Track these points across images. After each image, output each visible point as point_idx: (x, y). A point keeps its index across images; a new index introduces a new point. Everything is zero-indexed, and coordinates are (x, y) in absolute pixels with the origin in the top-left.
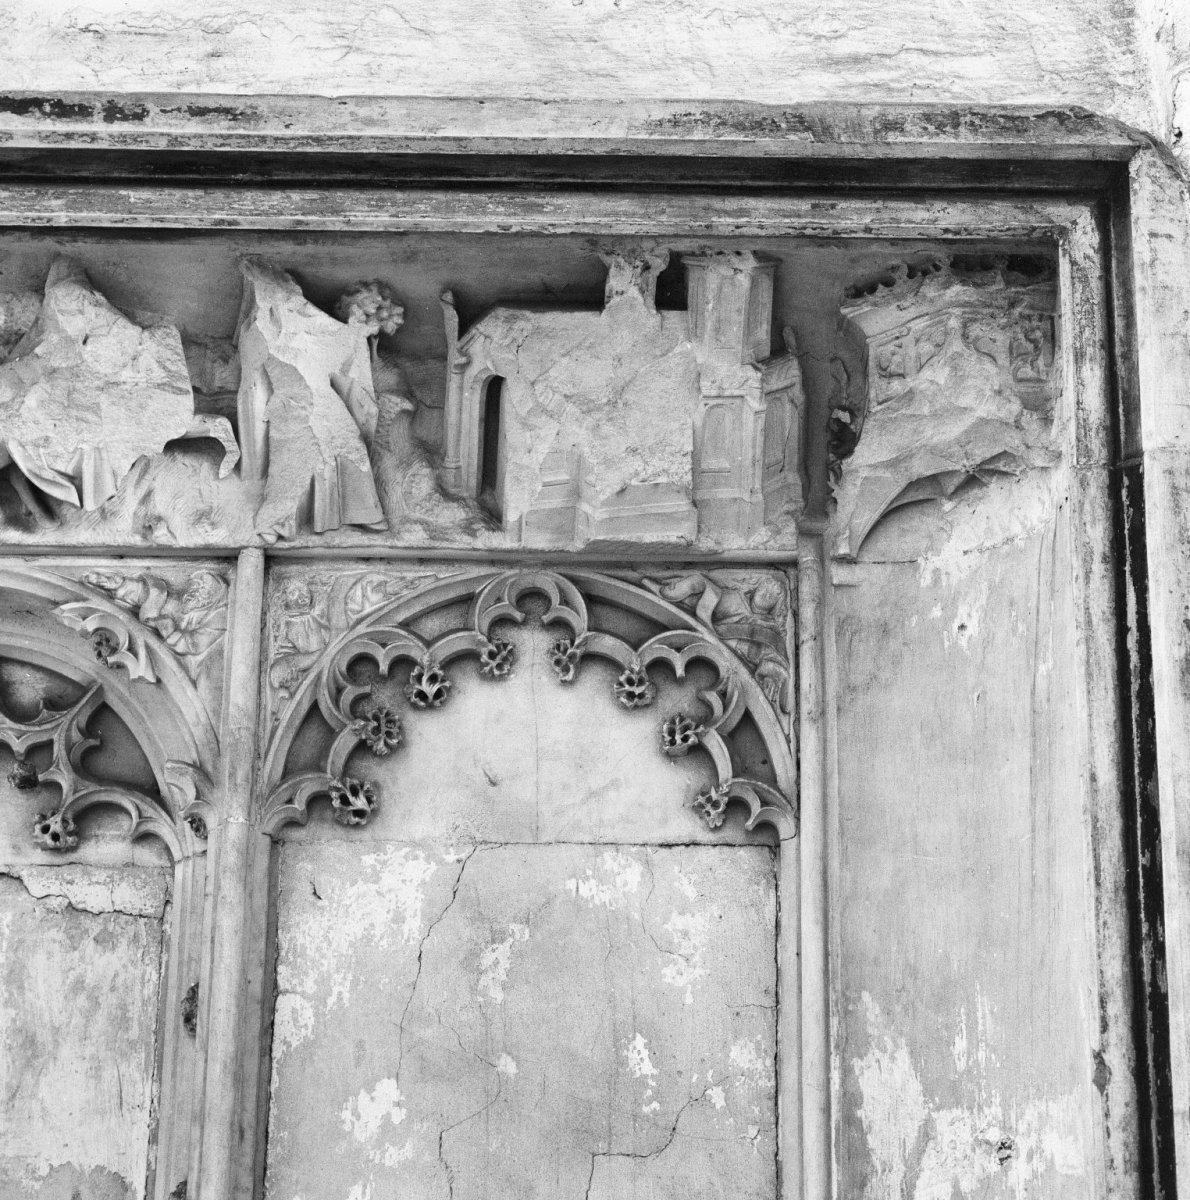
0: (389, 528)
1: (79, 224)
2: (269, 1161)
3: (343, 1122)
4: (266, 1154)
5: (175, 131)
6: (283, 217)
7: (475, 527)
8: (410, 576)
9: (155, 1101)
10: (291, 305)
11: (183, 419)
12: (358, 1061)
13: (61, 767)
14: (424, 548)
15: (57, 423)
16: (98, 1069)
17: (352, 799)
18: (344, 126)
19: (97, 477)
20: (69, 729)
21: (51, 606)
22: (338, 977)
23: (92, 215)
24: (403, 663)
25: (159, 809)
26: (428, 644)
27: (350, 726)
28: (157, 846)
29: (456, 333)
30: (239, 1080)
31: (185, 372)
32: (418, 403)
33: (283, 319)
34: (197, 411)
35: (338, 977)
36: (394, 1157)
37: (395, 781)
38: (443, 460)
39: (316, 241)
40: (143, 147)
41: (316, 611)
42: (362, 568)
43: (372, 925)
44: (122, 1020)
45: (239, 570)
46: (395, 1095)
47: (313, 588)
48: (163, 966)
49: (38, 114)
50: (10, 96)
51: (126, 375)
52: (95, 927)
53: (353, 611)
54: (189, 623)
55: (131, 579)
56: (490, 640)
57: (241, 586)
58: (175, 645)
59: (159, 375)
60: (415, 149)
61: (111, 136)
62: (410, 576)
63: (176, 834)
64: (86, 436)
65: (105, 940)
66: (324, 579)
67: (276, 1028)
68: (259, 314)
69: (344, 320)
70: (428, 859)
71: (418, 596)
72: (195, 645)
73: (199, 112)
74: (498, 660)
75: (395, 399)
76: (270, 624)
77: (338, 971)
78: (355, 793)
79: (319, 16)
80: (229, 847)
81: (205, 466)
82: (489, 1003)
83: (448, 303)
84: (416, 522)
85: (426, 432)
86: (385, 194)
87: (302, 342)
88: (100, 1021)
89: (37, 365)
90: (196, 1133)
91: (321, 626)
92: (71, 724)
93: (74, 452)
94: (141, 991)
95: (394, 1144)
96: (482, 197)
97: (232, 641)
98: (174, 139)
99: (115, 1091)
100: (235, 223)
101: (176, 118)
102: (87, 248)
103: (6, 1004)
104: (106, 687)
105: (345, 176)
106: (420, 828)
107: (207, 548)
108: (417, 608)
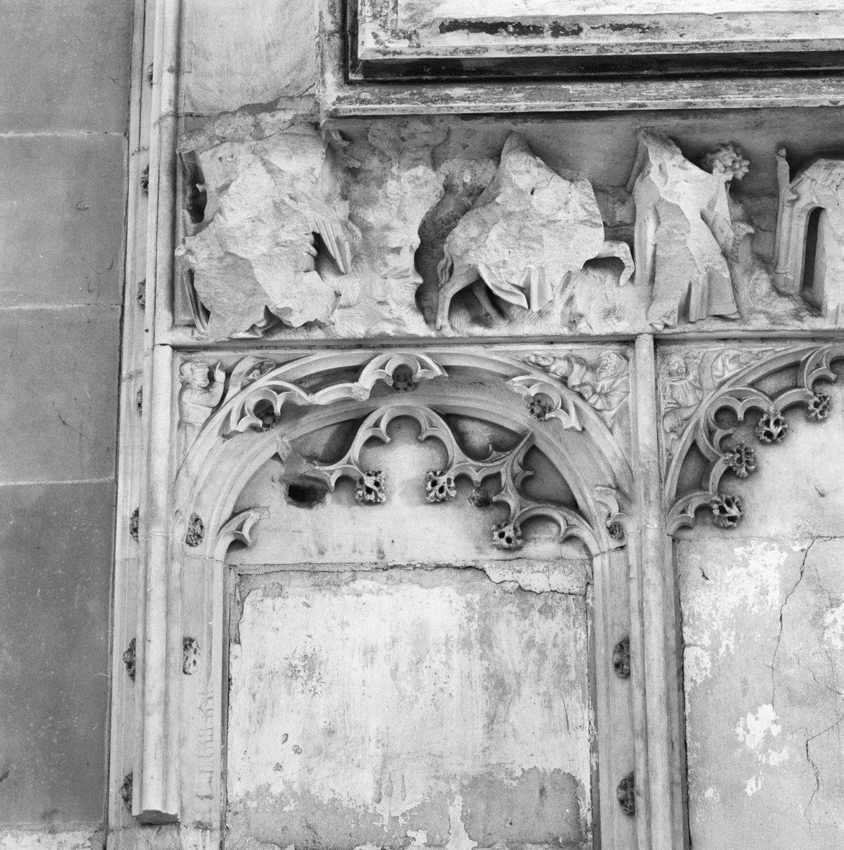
0: (741, 317)
1: (534, 110)
2: (689, 764)
3: (738, 735)
4: (686, 759)
5: (602, 42)
6: (677, 100)
7: (802, 314)
8: (755, 350)
9: (592, 722)
10: (674, 162)
11: (597, 244)
12: (744, 692)
13: (509, 491)
14: (767, 331)
15: (511, 250)
16: (550, 701)
17: (728, 509)
18: (721, 34)
19: (541, 288)
20: (512, 465)
21: (502, 379)
22: (725, 634)
23: (543, 103)
24: (754, 412)
25: (581, 519)
26: (773, 397)
27: (723, 458)
29: (788, 178)
30: (669, 709)
31: (598, 212)
32: (757, 227)
33: (669, 172)
34: (606, 239)
35: (725, 634)
36: (776, 759)
38: (775, 268)
39: (695, 116)
40: (580, 54)
41: (691, 378)
42: (722, 345)
43: (746, 597)
44: (563, 667)
45: (637, 350)
46: (773, 716)
47: (687, 360)
48: (589, 628)
49: (505, 33)
50: (484, 21)
51: (561, 215)
52: (539, 603)
53: (717, 377)
54: (603, 388)
55: (560, 359)
56: (815, 394)
57: (640, 361)
58: (595, 403)
59: (582, 215)
60: (772, 49)
61: (557, 47)
62: (755, 350)
63: (594, 536)
64: (533, 259)
65: (546, 611)
66: (695, 354)
67: (685, 670)
68: (652, 169)
69: (710, 171)
70: (781, 549)
71: (762, 365)
72: (609, 403)
73: (618, 28)
74: (821, 407)
75: (743, 226)
76: (660, 388)
77: (724, 630)
78: (729, 505)
80: (649, 545)
81: (609, 278)
82: (832, 650)
83: (782, 156)
84: (760, 312)
85: (765, 249)
86: (750, 82)
87: (683, 187)
88: (548, 669)
89: (497, 210)
90: (639, 745)
91: (696, 388)
92: (513, 461)
93: (524, 271)
94: (575, 647)
95: (775, 750)
96: (819, 81)
97: (636, 400)
98: (601, 48)
99: (563, 716)
100: (644, 105)
101: (602, 32)
102: (532, 127)
103: (481, 658)
104: (536, 434)
105: (720, 69)
106: (773, 528)
107: (614, 335)
108: (761, 373)
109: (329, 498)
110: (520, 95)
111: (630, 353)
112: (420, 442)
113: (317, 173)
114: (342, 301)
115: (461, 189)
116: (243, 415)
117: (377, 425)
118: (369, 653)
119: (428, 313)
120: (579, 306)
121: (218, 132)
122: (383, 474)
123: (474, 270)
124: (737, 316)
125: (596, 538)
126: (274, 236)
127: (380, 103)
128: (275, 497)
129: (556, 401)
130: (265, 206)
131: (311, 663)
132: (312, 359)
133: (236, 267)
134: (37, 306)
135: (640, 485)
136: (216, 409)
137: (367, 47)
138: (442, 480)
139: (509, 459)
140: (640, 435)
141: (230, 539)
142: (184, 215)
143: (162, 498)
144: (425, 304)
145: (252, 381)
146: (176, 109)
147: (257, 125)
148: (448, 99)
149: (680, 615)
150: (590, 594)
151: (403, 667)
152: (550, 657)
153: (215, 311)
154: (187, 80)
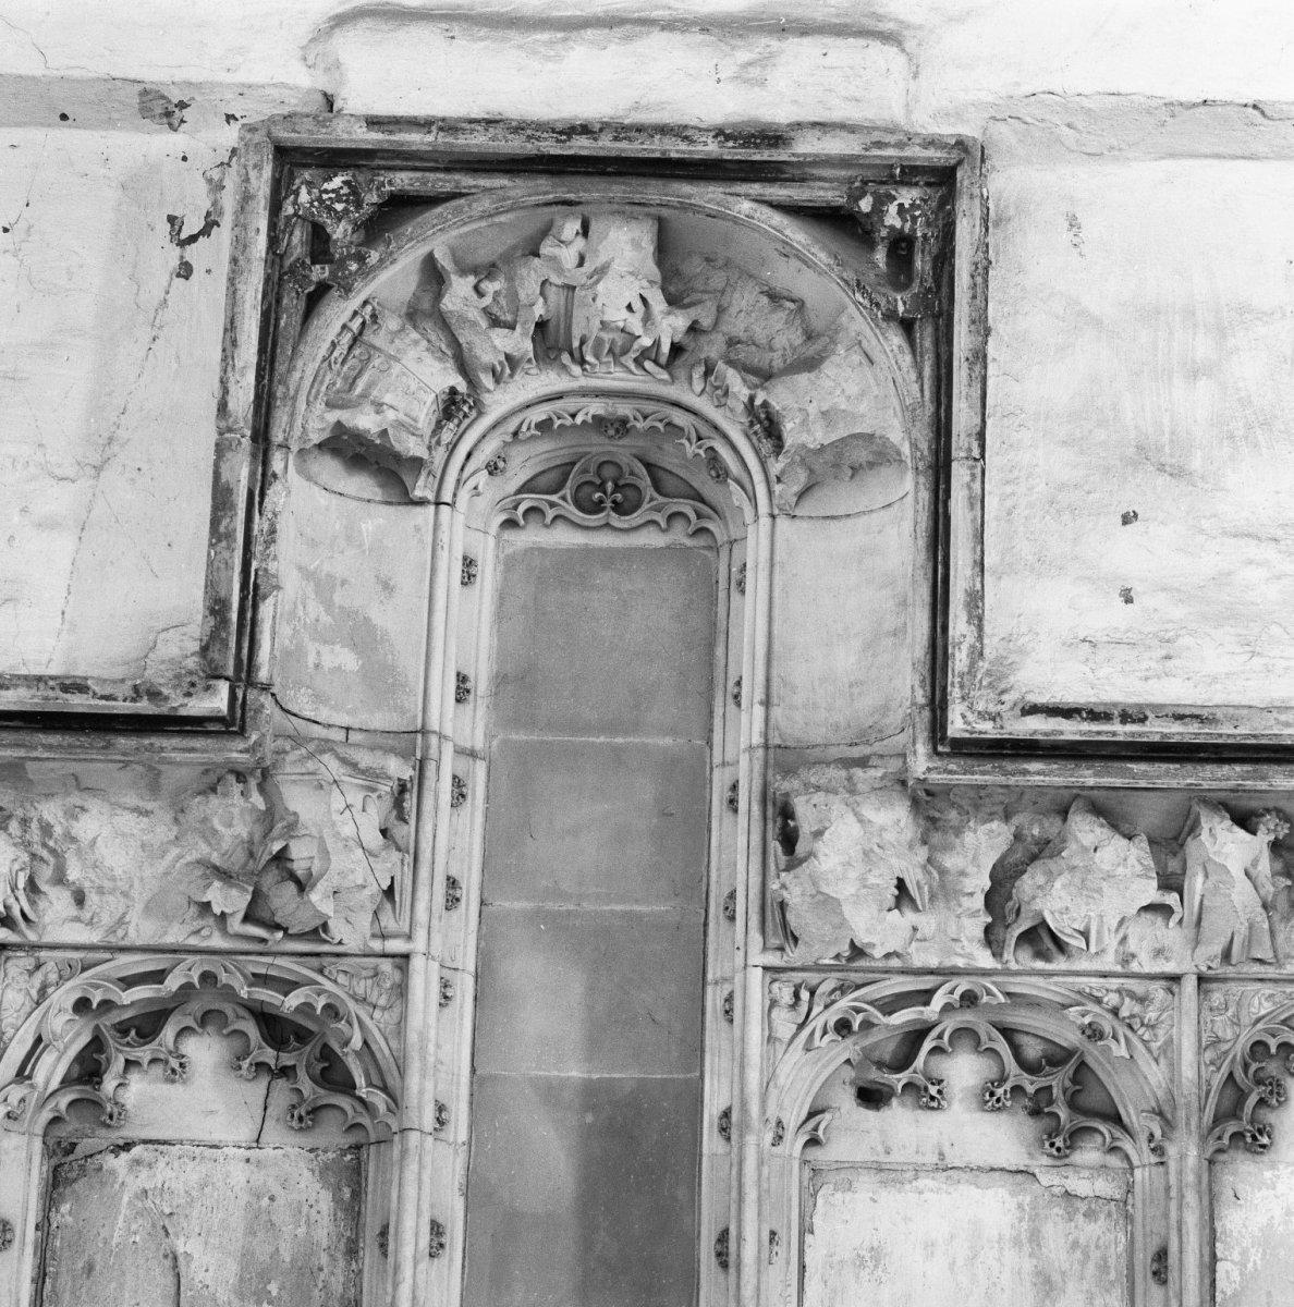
5: (1166, 730)
8: (1288, 990)
10: (1222, 825)
11: (1150, 892)
17: (1259, 1137)
27: (1256, 1091)
28: (1120, 1155)
31: (1153, 866)
35: (1253, 1251)
37: (1282, 1122)
40: (1145, 739)
41: (1229, 1013)
42: (1259, 985)
44: (1104, 1267)
52: (1083, 1207)
57: (1185, 1000)
59: (1139, 868)
65: (1090, 1215)
69: (1254, 833)
73: (1180, 717)
78: (1261, 1134)
79: (1232, 630)
81: (1159, 920)
87: (1230, 848)
88: (1091, 1268)
89: (1063, 863)
97: (1180, 1034)
98: (1164, 735)
109: (894, 1102)
110: (1090, 772)
111: (1175, 988)
112: (979, 1052)
113: (902, 824)
114: (919, 935)
115: (1029, 839)
116: (825, 1033)
117: (940, 1037)
118: (930, 1247)
119: (994, 947)
120: (1132, 946)
121: (813, 780)
122: (945, 1083)
123: (1040, 914)
124: (1273, 961)
125: (1139, 1152)
126: (863, 880)
127: (964, 774)
128: (845, 1100)
129: (1107, 1029)
130: (855, 853)
131: (877, 1254)
132: (888, 982)
133: (826, 904)
134: (628, 908)
135: (1182, 1114)
136: (801, 1026)
137: (956, 727)
138: (1000, 1092)
139: (1060, 1075)
140: (1184, 1068)
141: (806, 1138)
142: (775, 846)
143: (754, 1109)
144: (992, 938)
145: (833, 1002)
146: (767, 740)
147: (850, 779)
148: (1025, 772)
149: (1213, 1231)
150: (1130, 1201)
151: (960, 1262)
152: (1092, 1257)
153: (803, 938)
154: (776, 712)
